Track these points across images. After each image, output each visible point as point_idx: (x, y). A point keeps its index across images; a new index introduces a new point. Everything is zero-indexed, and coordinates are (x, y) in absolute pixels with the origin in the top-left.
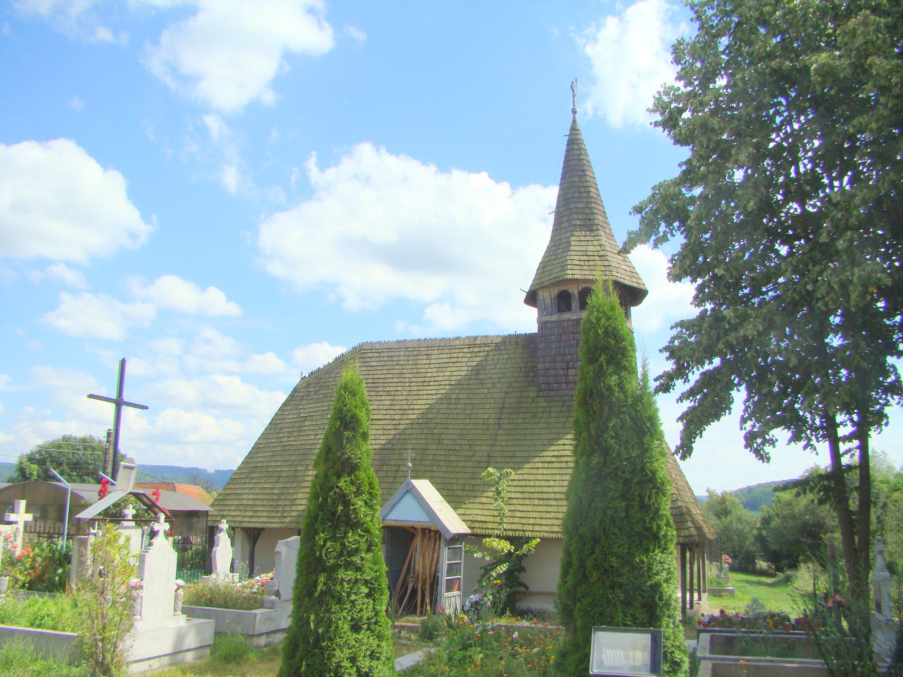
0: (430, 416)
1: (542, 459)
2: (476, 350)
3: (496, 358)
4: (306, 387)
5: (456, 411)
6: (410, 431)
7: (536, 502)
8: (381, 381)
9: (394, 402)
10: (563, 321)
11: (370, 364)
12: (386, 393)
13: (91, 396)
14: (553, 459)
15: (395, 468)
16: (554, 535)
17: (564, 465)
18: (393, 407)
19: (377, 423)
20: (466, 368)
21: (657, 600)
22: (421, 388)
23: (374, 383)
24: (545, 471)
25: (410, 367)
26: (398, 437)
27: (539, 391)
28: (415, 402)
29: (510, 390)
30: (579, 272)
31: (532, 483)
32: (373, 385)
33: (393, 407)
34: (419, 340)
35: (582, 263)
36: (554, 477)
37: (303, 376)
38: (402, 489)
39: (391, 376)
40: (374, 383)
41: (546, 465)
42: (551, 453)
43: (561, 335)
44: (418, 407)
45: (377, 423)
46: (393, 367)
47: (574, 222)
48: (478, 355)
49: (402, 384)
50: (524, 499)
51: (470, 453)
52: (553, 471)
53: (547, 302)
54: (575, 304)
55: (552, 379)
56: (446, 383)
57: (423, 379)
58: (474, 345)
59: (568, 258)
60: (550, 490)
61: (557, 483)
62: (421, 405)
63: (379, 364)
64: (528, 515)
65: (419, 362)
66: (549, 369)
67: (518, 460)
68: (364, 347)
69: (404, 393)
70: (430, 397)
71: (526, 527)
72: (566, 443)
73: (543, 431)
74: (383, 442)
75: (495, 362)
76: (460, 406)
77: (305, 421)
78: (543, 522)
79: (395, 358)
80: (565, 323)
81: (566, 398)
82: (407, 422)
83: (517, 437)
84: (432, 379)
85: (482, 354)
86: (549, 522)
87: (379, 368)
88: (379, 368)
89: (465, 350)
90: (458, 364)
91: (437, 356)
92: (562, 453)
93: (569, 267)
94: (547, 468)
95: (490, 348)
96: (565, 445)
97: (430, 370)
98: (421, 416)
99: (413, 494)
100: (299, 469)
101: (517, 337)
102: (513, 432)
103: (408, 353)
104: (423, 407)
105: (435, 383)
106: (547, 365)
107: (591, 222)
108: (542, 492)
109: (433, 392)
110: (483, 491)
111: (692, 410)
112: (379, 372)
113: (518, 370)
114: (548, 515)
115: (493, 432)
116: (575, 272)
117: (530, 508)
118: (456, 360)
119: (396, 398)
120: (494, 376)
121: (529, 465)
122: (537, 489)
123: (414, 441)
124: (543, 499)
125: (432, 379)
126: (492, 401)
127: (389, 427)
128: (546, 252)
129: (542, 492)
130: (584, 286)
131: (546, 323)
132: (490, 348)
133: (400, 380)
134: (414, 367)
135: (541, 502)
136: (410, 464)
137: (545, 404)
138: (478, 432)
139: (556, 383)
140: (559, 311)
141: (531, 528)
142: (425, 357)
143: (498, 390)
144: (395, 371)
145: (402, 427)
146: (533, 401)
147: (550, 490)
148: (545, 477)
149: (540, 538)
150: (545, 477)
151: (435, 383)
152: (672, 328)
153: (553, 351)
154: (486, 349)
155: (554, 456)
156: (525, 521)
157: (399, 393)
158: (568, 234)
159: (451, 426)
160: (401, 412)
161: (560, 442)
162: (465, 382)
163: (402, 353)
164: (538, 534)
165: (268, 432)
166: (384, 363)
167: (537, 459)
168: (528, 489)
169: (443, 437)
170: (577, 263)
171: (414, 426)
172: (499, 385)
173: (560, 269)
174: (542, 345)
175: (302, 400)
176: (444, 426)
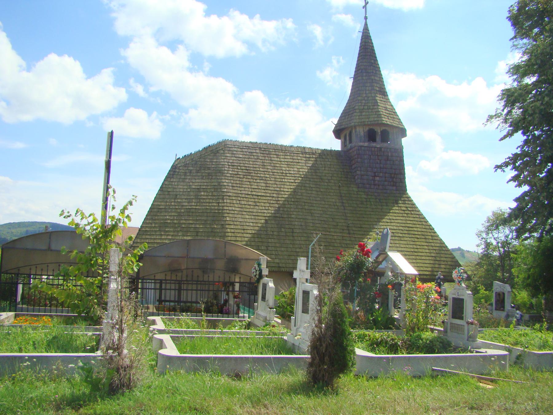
2: (308, 156)
4: (185, 166)
9: (268, 185)
10: (372, 147)
19: (262, 198)
21: (318, 358)
22: (283, 177)
34: (266, 144)
40: (247, 170)
43: (371, 156)
44: (287, 190)
48: (310, 159)
54: (378, 138)
58: (306, 153)
63: (244, 156)
65: (273, 159)
66: (364, 175)
68: (228, 143)
77: (201, 192)
80: (373, 149)
88: (246, 159)
96: (387, 222)
103: (262, 152)
106: (362, 172)
109: (292, 181)
111: (525, 194)
127: (271, 202)
128: (347, 104)
130: (384, 128)
137: (365, 197)
139: (368, 184)
142: (275, 156)
154: (314, 156)
161: (384, 220)
163: (258, 151)
169: (313, 211)
172: (333, 181)
176: (310, 205)
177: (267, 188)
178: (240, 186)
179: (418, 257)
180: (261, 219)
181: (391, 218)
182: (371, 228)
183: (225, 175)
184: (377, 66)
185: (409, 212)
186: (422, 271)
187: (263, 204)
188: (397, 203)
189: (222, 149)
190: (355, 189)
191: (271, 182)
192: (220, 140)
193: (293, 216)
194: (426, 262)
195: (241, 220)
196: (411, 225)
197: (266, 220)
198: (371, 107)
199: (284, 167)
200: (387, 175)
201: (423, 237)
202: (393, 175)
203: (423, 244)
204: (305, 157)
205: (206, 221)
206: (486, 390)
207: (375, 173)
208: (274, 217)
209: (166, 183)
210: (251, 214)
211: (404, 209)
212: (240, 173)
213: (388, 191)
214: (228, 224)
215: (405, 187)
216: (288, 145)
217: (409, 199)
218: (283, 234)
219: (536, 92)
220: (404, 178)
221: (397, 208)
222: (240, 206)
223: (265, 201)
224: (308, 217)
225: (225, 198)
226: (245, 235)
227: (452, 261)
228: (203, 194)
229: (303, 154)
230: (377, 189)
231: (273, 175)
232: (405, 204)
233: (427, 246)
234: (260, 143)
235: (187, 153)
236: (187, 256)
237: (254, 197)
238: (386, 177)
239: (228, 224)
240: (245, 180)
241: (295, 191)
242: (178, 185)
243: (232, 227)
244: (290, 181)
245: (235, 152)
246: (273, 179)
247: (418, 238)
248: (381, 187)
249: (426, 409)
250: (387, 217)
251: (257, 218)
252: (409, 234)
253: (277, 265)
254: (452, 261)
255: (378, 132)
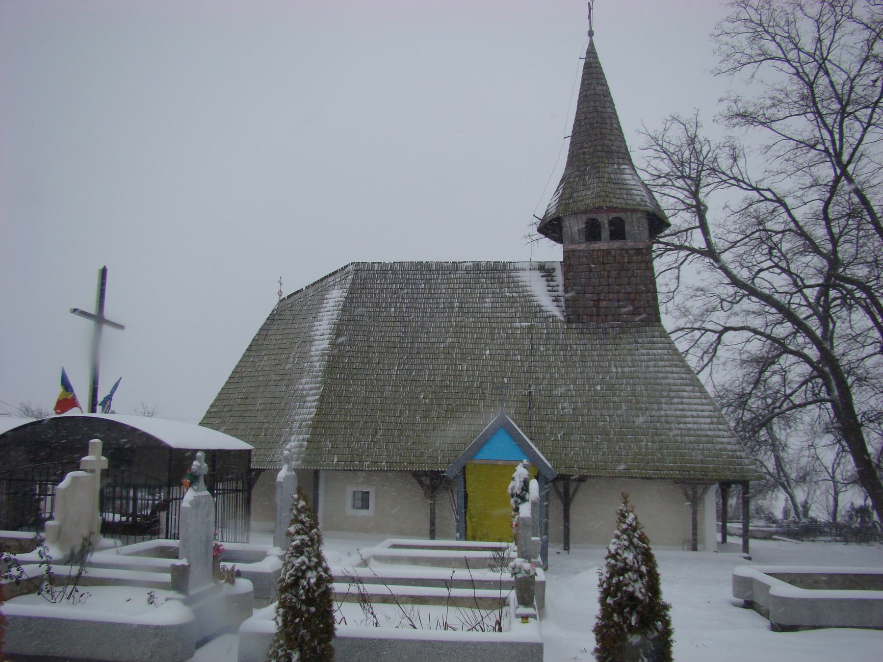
54: (605, 233)
184: (604, 81)
205: (670, 390)
206: (709, 460)
219: (301, 620)
238: (609, 285)
249: (663, 159)
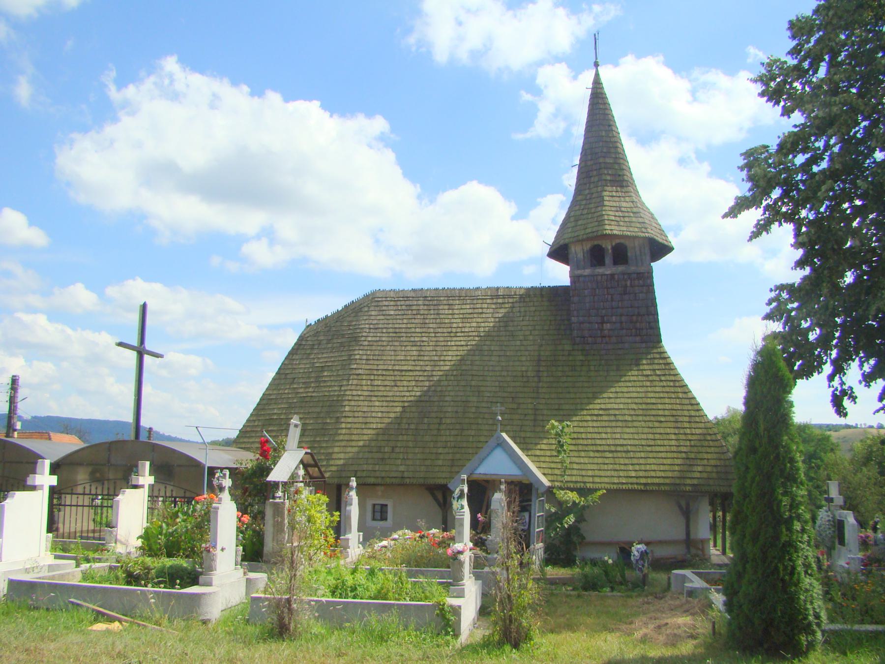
0: (464, 368)
1: (590, 412)
2: (500, 301)
3: (523, 309)
4: (314, 335)
5: (491, 363)
6: (446, 383)
7: (592, 454)
8: (403, 330)
9: (422, 353)
10: (597, 275)
11: (387, 313)
12: (411, 343)
13: (120, 344)
14: (601, 412)
15: (438, 421)
16: (615, 487)
17: (612, 418)
18: (422, 358)
19: (407, 374)
20: (493, 320)
22: (449, 339)
23: (396, 333)
24: (595, 424)
25: (432, 316)
26: (433, 388)
27: (574, 344)
28: (445, 353)
29: (544, 342)
30: (616, 228)
31: (583, 436)
32: (395, 335)
33: (422, 358)
34: (437, 289)
35: (618, 219)
36: (604, 430)
37: (308, 324)
38: (492, 442)
39: (414, 325)
40: (396, 333)
41: (595, 418)
42: (598, 407)
44: (450, 358)
45: (407, 374)
46: (413, 317)
47: (604, 177)
48: (503, 306)
49: (427, 335)
50: (578, 451)
51: (515, 406)
52: (604, 424)
53: (579, 255)
54: (608, 260)
55: (586, 333)
56: (474, 334)
57: (450, 330)
58: (498, 297)
59: (604, 213)
60: (604, 442)
61: (609, 436)
62: (452, 356)
63: (397, 312)
64: (585, 467)
65: (441, 312)
67: (565, 412)
68: (378, 295)
69: (431, 344)
70: (461, 348)
71: (586, 479)
72: (611, 396)
73: (586, 385)
74: (418, 394)
75: (522, 314)
76: (493, 358)
77: (323, 371)
78: (602, 473)
79: (414, 307)
81: (603, 352)
82: (441, 373)
83: (560, 390)
84: (459, 330)
85: (507, 306)
86: (609, 473)
87: (398, 317)
88: (398, 317)
89: (488, 301)
90: (484, 316)
91: (459, 307)
92: (609, 406)
93: (607, 222)
94: (596, 421)
95: (515, 300)
96: (610, 398)
97: (455, 321)
98: (454, 368)
99: (504, 450)
100: (328, 421)
101: (542, 289)
102: (555, 385)
103: (427, 303)
104: (454, 358)
105: (463, 334)
106: (581, 318)
107: (621, 178)
108: (596, 445)
109: (463, 343)
110: (536, 444)
112: (398, 321)
113: (548, 322)
114: (606, 467)
115: (534, 384)
116: (613, 228)
117: (586, 460)
118: (480, 311)
119: (423, 348)
120: (524, 328)
121: (578, 418)
122: (590, 442)
123: (452, 394)
124: (598, 451)
125: (459, 330)
126: (527, 353)
127: (421, 378)
129: (596, 445)
130: (618, 241)
131: (579, 276)
132: (515, 300)
133: (424, 330)
134: (436, 316)
135: (597, 455)
136: (500, 418)
137: (581, 358)
138: (518, 384)
139: (591, 337)
140: (592, 266)
141: (591, 479)
142: (446, 307)
143: (532, 343)
144: (416, 321)
145: (435, 379)
146: (569, 355)
147: (604, 442)
148: (596, 430)
149: (606, 490)
150: (596, 430)
151: (463, 334)
152: (771, 290)
153: (587, 305)
154: (511, 300)
155: (601, 409)
156: (584, 473)
157: (426, 344)
158: (599, 189)
159: (489, 378)
160: (432, 363)
161: (605, 395)
162: (495, 334)
163: (420, 303)
164: (603, 485)
165: (277, 382)
166: (403, 312)
167: (585, 412)
168: (581, 442)
169: (482, 389)
170: (613, 218)
171: (449, 378)
172: (531, 338)
173: (596, 224)
174: (576, 299)
175: (312, 349)
176: (481, 378)
177: (420, 358)
178: (379, 358)
179: (651, 455)
180: (397, 406)
181: (618, 390)
182: (577, 409)
183: (361, 343)
185: (657, 378)
186: (663, 477)
187: (405, 383)
188: (638, 365)
189: (367, 306)
190: (568, 347)
191: (428, 348)
192: (367, 290)
193: (447, 399)
194: (665, 463)
195: (365, 409)
196: (653, 401)
197: (403, 407)
198: (593, 211)
199: (457, 322)
200: (624, 319)
201: (672, 419)
202: (634, 318)
203: (668, 431)
204: (496, 303)
207: (602, 317)
208: (419, 401)
209: (286, 362)
210: (384, 399)
211: (649, 373)
212: (384, 339)
213: (626, 345)
214: (345, 417)
215: (659, 335)
216: (471, 288)
217: (663, 357)
218: (426, 427)
220: (657, 321)
221: (636, 373)
222: (370, 388)
223: (410, 378)
224: (471, 399)
225: (351, 378)
226: (365, 431)
227: (720, 459)
228: (325, 374)
229: (492, 299)
230: (606, 343)
231: (435, 336)
232: (654, 364)
233: (675, 434)
234: (427, 290)
235: (321, 315)
236: (109, 461)
237: (396, 373)
239: (345, 417)
240: (388, 348)
241: (462, 360)
242: (299, 364)
243: (350, 420)
244: (459, 343)
245: (384, 308)
246: (433, 343)
247: (661, 422)
248: (614, 340)
250: (613, 390)
251: (391, 404)
252: (645, 415)
253: (400, 475)
254: (720, 459)
255: (608, 250)
